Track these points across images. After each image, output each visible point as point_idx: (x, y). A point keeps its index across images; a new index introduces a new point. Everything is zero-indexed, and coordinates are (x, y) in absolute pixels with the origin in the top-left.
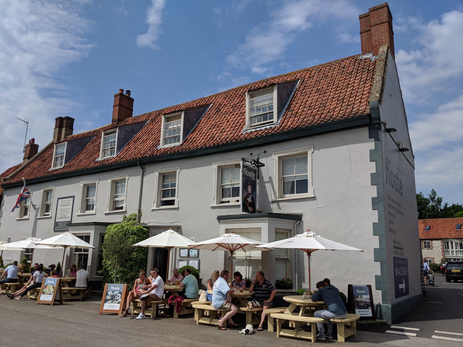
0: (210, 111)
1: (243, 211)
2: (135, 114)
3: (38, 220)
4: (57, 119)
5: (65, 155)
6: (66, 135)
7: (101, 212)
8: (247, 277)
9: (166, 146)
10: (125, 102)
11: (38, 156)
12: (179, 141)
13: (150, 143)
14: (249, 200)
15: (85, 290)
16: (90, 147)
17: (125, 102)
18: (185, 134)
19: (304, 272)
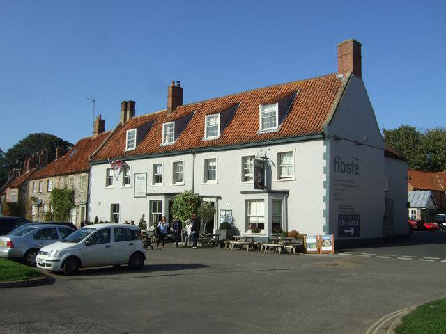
0: (239, 111)
1: (255, 188)
2: (184, 104)
3: (252, 204)
4: (122, 103)
5: (277, 115)
6: (131, 116)
7: (167, 186)
8: (37, 184)
9: (130, 149)
10: (177, 93)
11: (111, 136)
12: (275, 126)
13: (197, 133)
14: (259, 181)
15: (7, 187)
16: (153, 132)
17: (177, 93)
18: (221, 131)
19: (412, 245)
